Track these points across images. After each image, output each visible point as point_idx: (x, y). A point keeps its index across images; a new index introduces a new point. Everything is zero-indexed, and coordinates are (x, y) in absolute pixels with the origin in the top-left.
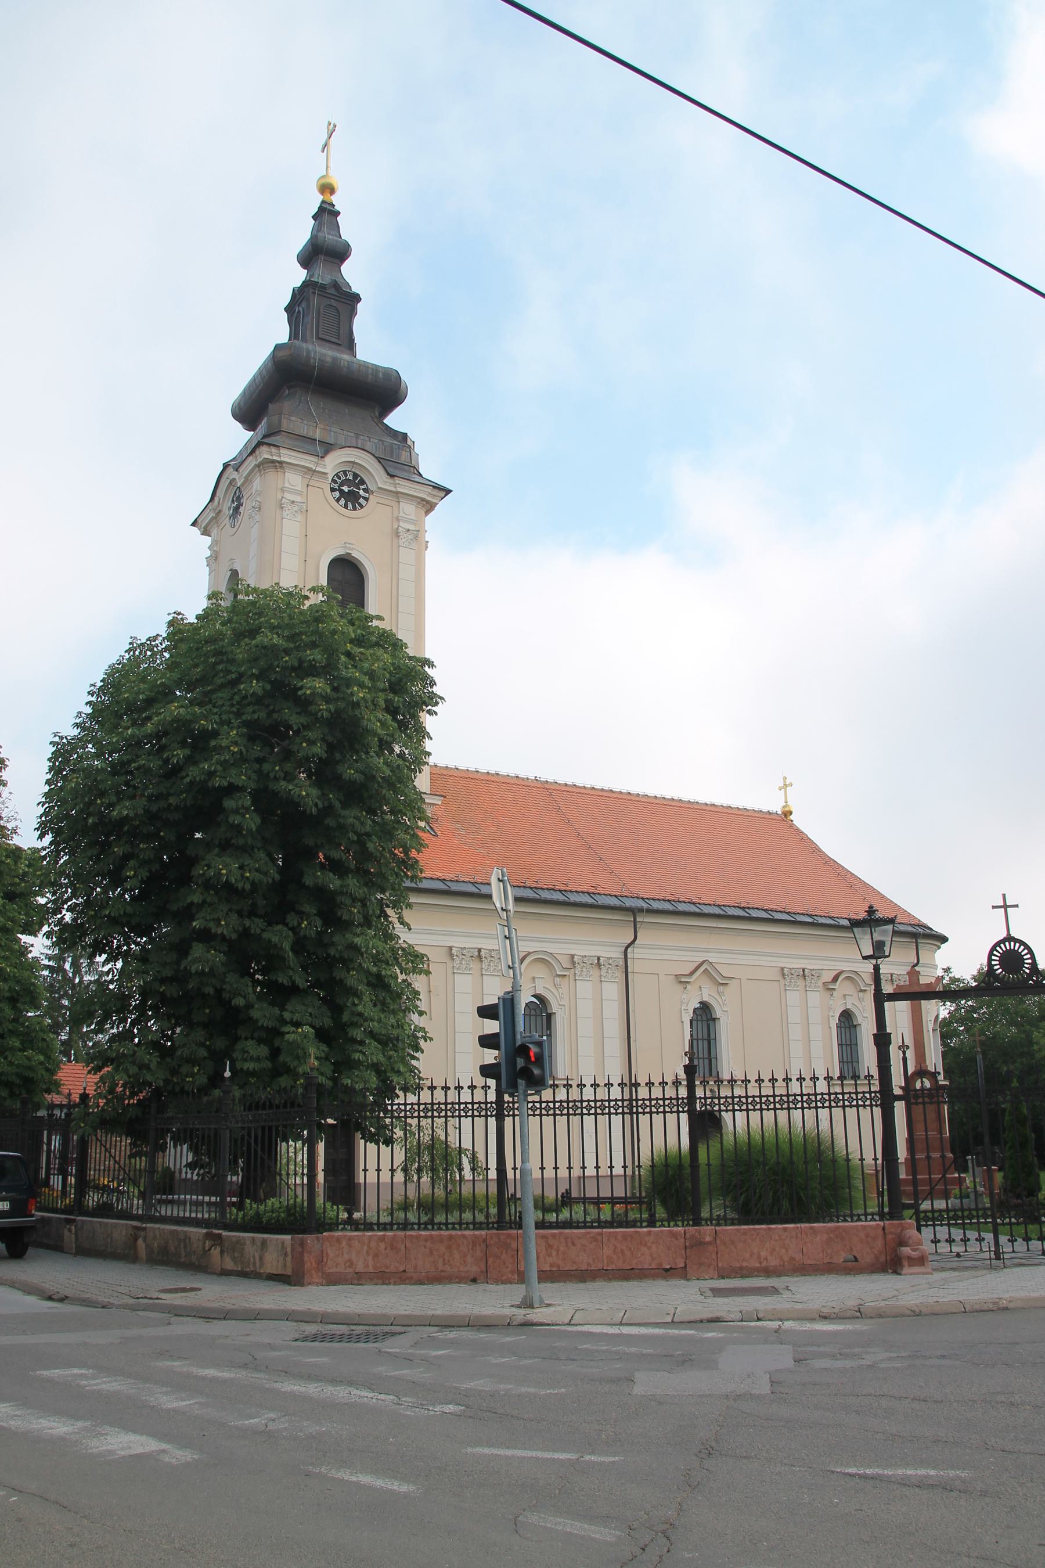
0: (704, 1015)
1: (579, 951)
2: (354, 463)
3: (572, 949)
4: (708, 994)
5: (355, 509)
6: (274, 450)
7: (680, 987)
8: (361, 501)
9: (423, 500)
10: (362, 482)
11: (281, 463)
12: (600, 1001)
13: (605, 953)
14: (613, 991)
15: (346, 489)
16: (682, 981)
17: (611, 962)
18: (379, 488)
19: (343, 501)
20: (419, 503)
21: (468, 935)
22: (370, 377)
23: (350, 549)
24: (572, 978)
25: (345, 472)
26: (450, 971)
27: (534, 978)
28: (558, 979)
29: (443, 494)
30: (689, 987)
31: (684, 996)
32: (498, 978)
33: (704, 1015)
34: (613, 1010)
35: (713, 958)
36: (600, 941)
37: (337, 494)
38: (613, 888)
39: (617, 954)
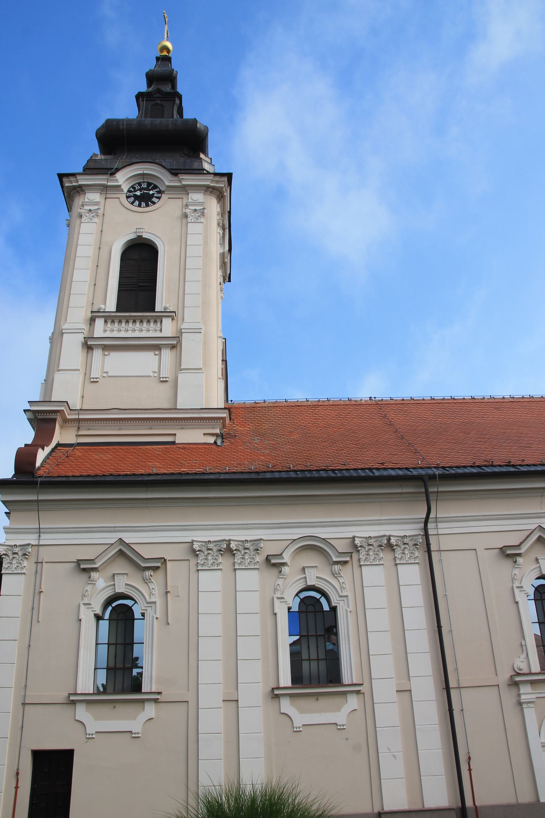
0: (121, 616)
1: (362, 532)
2: (143, 175)
3: (187, 536)
4: (317, 574)
5: (147, 205)
6: (72, 179)
7: (508, 563)
8: (154, 200)
9: (214, 188)
10: (155, 187)
11: (80, 186)
12: (232, 594)
13: (396, 531)
14: (412, 575)
15: (138, 193)
16: (509, 554)
17: (406, 541)
18: (168, 187)
19: (143, 204)
20: (206, 191)
21: (380, 523)
22: (170, 126)
23: (140, 232)
24: (355, 564)
25: (140, 184)
26: (193, 569)
27: (304, 569)
28: (336, 567)
29: (92, 165)
30: (520, 560)
31: (516, 571)
32: (256, 572)
33: (121, 616)
34: (415, 596)
35: (129, 538)
36: (395, 521)
37: (132, 199)
38: (468, 461)
39: (413, 530)
